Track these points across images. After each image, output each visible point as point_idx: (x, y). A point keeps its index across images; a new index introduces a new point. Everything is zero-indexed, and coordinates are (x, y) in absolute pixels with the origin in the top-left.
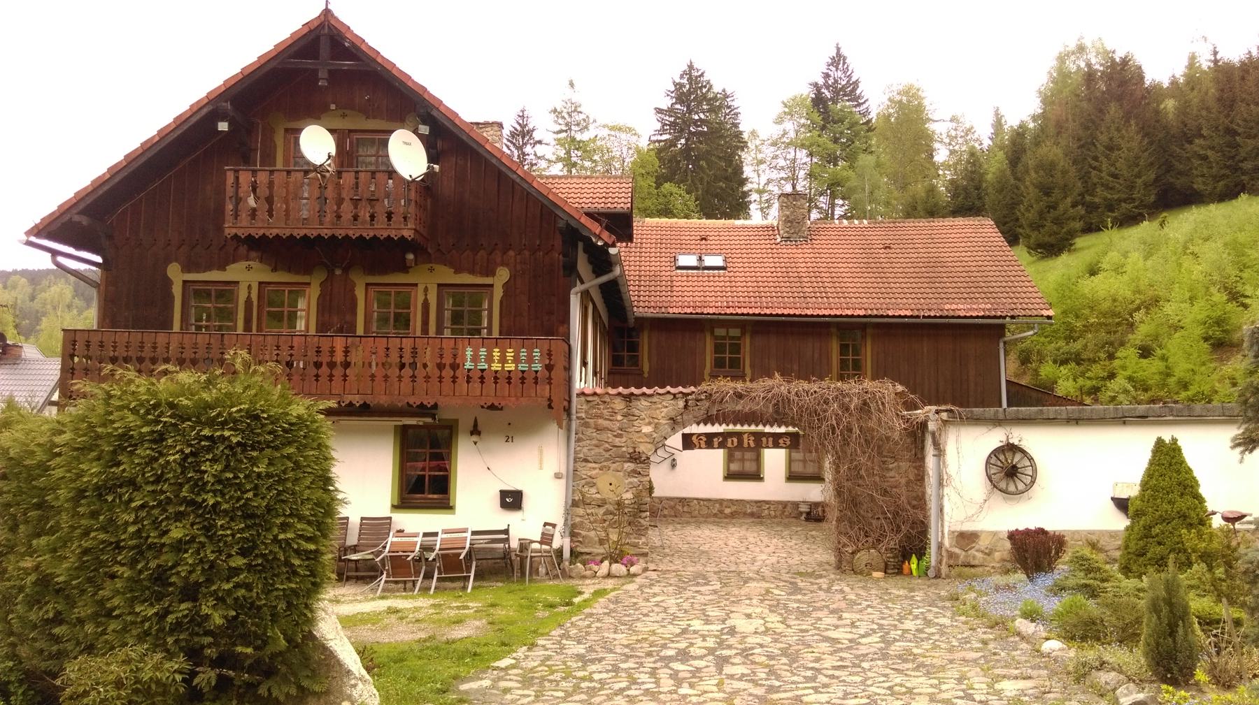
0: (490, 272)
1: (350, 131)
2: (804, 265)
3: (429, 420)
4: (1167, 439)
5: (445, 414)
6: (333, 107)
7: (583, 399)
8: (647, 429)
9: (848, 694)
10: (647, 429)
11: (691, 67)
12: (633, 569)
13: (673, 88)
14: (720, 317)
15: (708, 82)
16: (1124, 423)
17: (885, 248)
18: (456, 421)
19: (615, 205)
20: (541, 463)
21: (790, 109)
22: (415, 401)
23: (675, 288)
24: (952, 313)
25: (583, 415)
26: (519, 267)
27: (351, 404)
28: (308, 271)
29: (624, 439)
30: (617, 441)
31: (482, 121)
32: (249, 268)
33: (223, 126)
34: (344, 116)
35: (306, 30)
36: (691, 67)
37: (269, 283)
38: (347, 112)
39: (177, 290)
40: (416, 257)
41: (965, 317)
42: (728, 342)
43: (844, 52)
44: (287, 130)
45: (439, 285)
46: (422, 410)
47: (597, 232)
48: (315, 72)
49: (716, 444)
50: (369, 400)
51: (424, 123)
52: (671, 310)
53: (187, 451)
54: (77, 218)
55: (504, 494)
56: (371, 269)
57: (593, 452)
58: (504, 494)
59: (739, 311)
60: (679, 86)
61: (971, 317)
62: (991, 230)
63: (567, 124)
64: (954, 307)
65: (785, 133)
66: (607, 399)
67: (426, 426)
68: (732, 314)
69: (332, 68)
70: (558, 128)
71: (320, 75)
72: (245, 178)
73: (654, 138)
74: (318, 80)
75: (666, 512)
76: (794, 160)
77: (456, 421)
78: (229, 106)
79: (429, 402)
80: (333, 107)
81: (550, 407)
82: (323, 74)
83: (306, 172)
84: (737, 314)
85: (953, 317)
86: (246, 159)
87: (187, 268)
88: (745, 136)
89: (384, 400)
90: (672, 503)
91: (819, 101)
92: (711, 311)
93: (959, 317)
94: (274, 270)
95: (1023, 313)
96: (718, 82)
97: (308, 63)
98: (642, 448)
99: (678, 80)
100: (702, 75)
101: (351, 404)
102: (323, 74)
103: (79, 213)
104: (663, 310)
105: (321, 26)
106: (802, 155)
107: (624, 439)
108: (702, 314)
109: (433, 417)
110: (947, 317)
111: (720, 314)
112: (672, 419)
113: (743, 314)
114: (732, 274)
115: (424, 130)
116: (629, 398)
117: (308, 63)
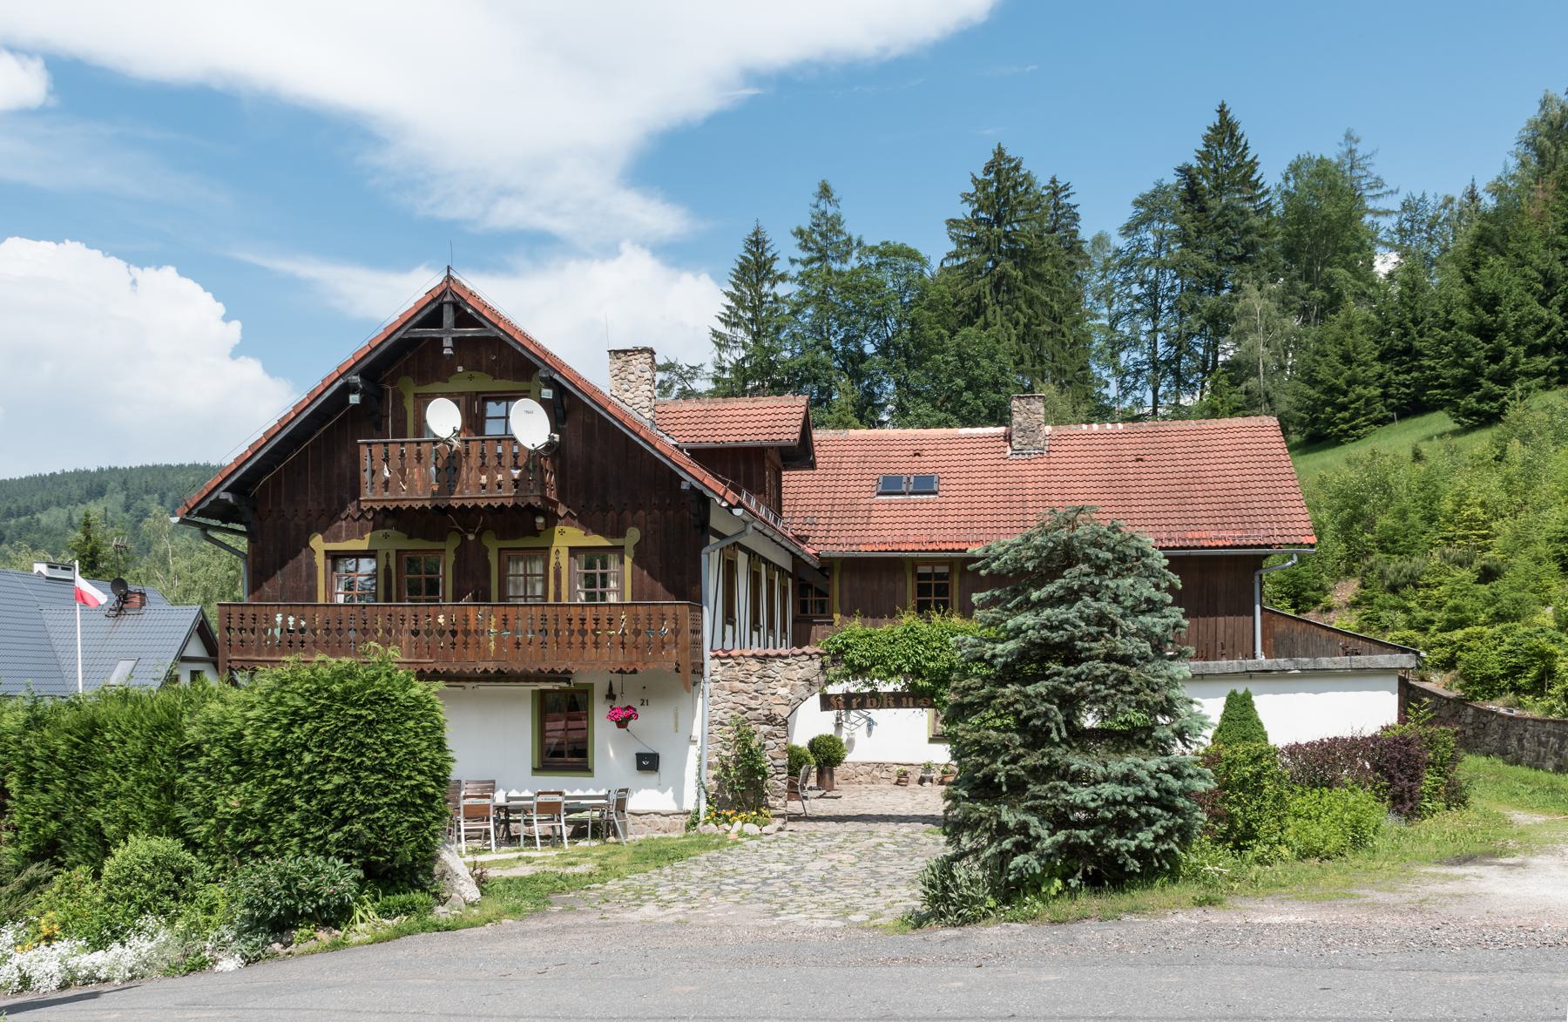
0: (620, 533)
1: (478, 393)
2: (1033, 485)
3: (564, 685)
4: (1240, 691)
5: (580, 679)
6: (460, 369)
7: (717, 661)
8: (783, 691)
9: (318, 718)
10: (783, 691)
11: (1000, 153)
12: (765, 830)
13: (972, 189)
14: (921, 555)
15: (1026, 177)
16: (1251, 677)
17: (1138, 460)
18: (592, 685)
19: (781, 436)
20: (676, 726)
21: (1150, 207)
22: (546, 667)
23: (872, 520)
24: (1195, 543)
25: (718, 678)
26: (649, 526)
27: (486, 671)
28: (443, 539)
29: (759, 702)
30: (753, 704)
31: (630, 347)
32: (386, 536)
33: (354, 399)
34: (471, 378)
35: (429, 298)
36: (1000, 153)
37: (406, 551)
38: (475, 374)
39: (320, 560)
40: (546, 521)
41: (1210, 547)
42: (933, 582)
43: (1235, 114)
44: (416, 395)
45: (570, 548)
46: (553, 676)
47: (721, 493)
48: (441, 340)
49: (855, 706)
50: (505, 668)
51: (548, 387)
52: (862, 548)
53: (340, 724)
54: (224, 496)
55: (640, 757)
56: (502, 535)
57: (728, 715)
58: (640, 757)
59: (943, 547)
60: (982, 185)
61: (1217, 547)
62: (1274, 433)
63: (820, 251)
64: (1197, 535)
65: (1141, 248)
66: (742, 660)
67: (561, 691)
68: (933, 551)
69: (457, 335)
70: (805, 255)
71: (445, 344)
72: (378, 451)
73: (946, 264)
74: (443, 348)
75: (861, 778)
76: (1155, 285)
77: (592, 685)
78: (356, 379)
79: (560, 668)
80: (460, 369)
81: (677, 670)
82: (448, 342)
83: (435, 443)
84: (940, 551)
85: (1195, 548)
86: (378, 429)
87: (326, 540)
88: (1087, 248)
89: (518, 668)
90: (869, 769)
91: (1192, 195)
92: (910, 547)
93: (1203, 547)
94: (410, 537)
95: (1280, 540)
96: (1040, 171)
97: (432, 332)
98: (777, 710)
99: (980, 176)
100: (1017, 168)
101: (486, 671)
102: (448, 342)
103: (225, 491)
104: (854, 548)
105: (444, 293)
106: (1168, 279)
107: (759, 702)
108: (899, 551)
109: (568, 681)
110: (1188, 548)
111: (920, 551)
112: (807, 680)
113: (947, 551)
114: (944, 499)
115: (547, 393)
116: (764, 659)
117: (432, 332)
